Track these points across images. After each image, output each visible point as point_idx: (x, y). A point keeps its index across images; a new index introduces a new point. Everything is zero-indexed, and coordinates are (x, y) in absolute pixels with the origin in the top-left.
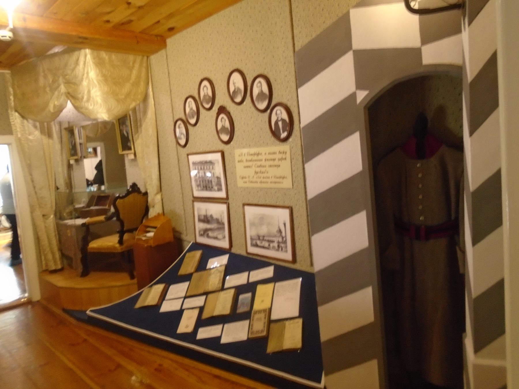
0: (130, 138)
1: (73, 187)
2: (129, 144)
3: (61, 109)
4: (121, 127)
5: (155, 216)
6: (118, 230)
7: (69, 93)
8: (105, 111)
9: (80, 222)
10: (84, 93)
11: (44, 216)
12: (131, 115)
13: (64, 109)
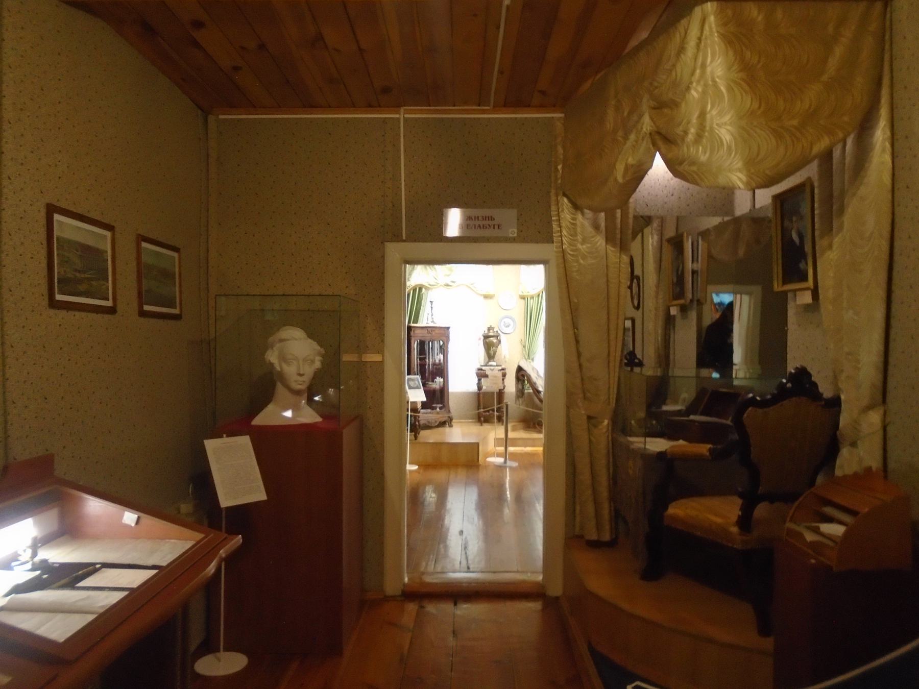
0: (808, 248)
1: (671, 366)
2: (802, 266)
3: (640, 171)
4: (787, 223)
5: (855, 475)
6: (740, 489)
7: (659, 133)
8: (740, 165)
9: (657, 445)
10: (689, 122)
11: (589, 418)
12: (816, 184)
13: (646, 172)
